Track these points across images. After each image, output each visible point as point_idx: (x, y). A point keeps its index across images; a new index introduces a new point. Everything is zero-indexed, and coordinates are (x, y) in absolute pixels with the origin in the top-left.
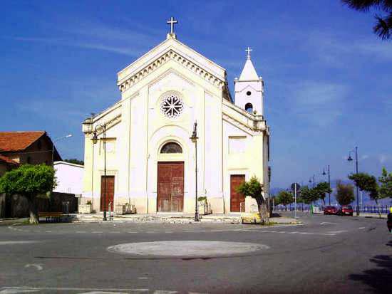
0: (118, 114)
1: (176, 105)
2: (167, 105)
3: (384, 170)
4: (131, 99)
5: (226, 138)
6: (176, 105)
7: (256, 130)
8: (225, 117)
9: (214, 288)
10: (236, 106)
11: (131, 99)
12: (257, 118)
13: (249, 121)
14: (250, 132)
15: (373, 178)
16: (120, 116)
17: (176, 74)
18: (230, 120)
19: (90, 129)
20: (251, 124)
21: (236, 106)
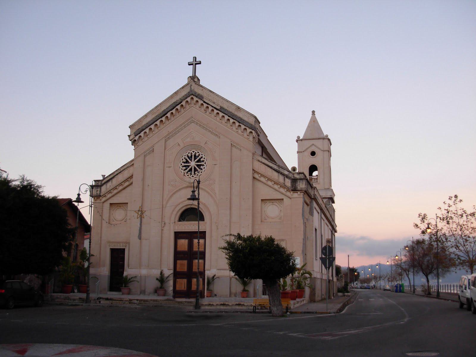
0: (129, 175)
1: (197, 162)
2: (187, 162)
3: (244, 235)
4: (145, 156)
5: (259, 202)
6: (197, 162)
7: (295, 190)
8: (257, 176)
9: (96, 349)
10: (103, 196)
11: (145, 156)
12: (297, 176)
13: (287, 180)
14: (288, 194)
15: (274, 239)
16: (131, 177)
17: (197, 123)
18: (262, 179)
19: (98, 192)
20: (288, 183)
21: (103, 196)
